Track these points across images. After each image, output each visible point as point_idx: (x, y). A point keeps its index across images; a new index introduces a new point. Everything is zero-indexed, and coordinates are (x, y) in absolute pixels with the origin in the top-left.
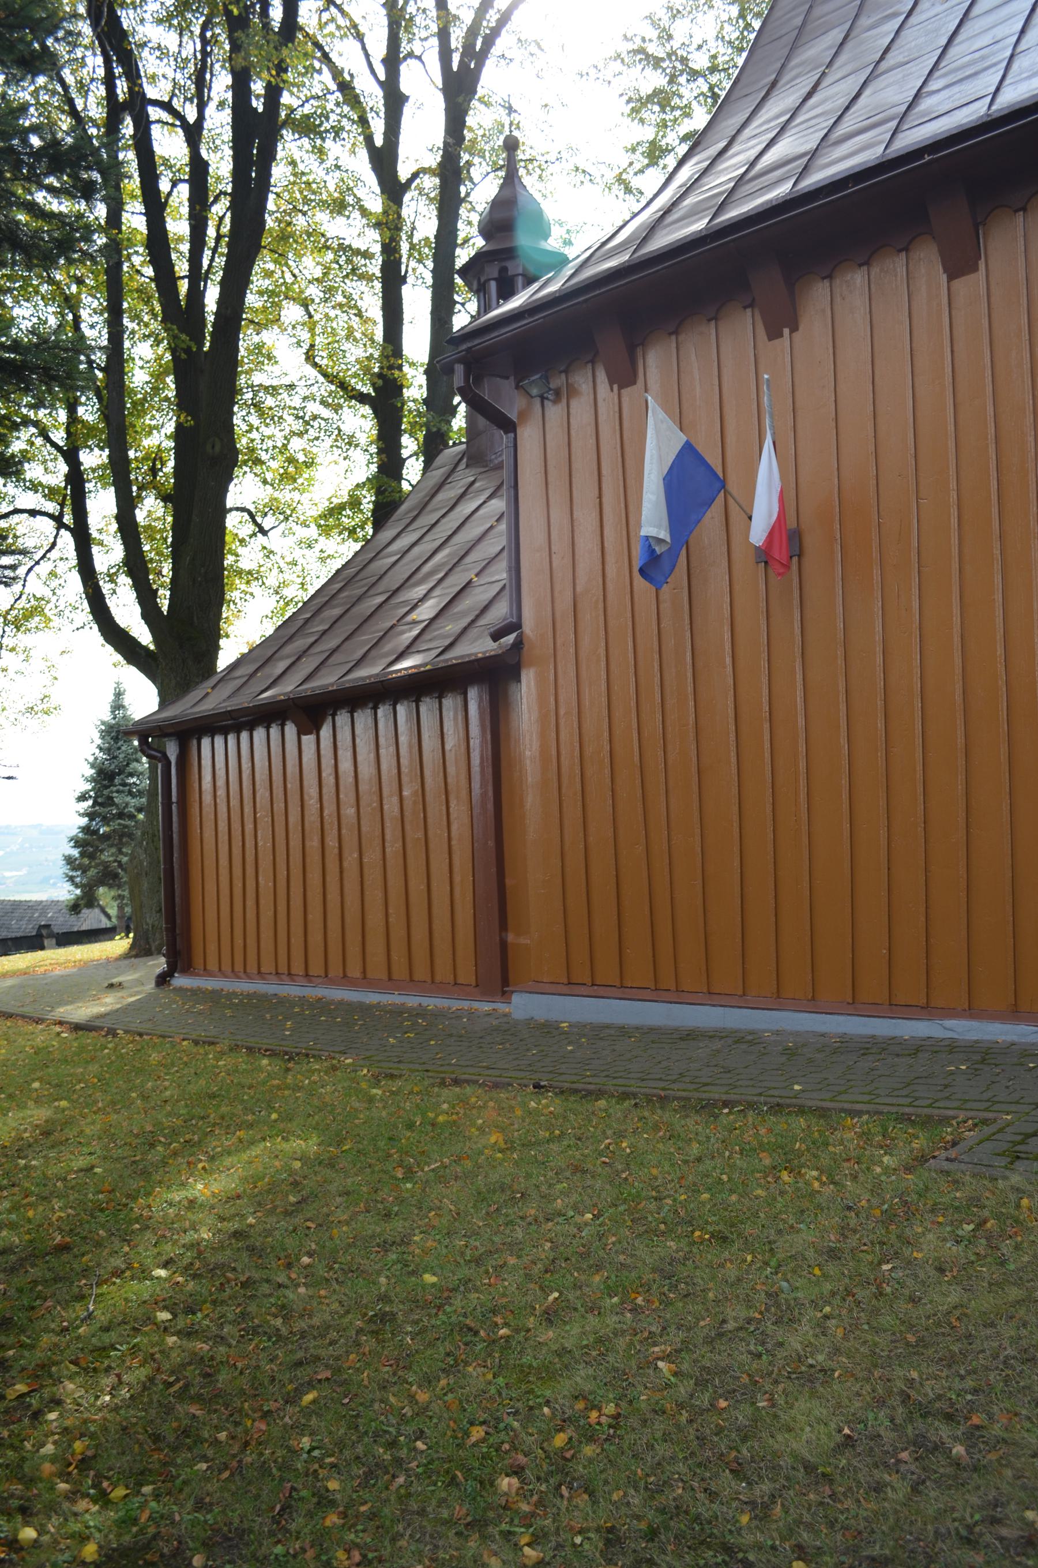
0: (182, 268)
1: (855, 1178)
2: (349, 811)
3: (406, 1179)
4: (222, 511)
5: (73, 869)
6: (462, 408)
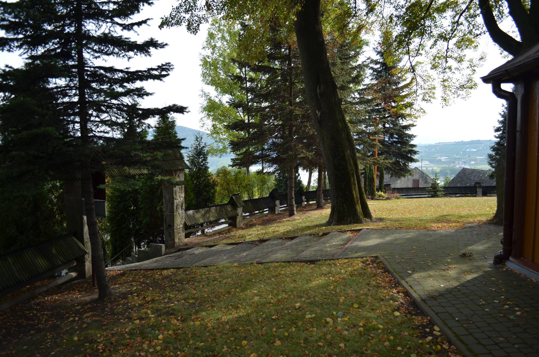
5: (491, 160)
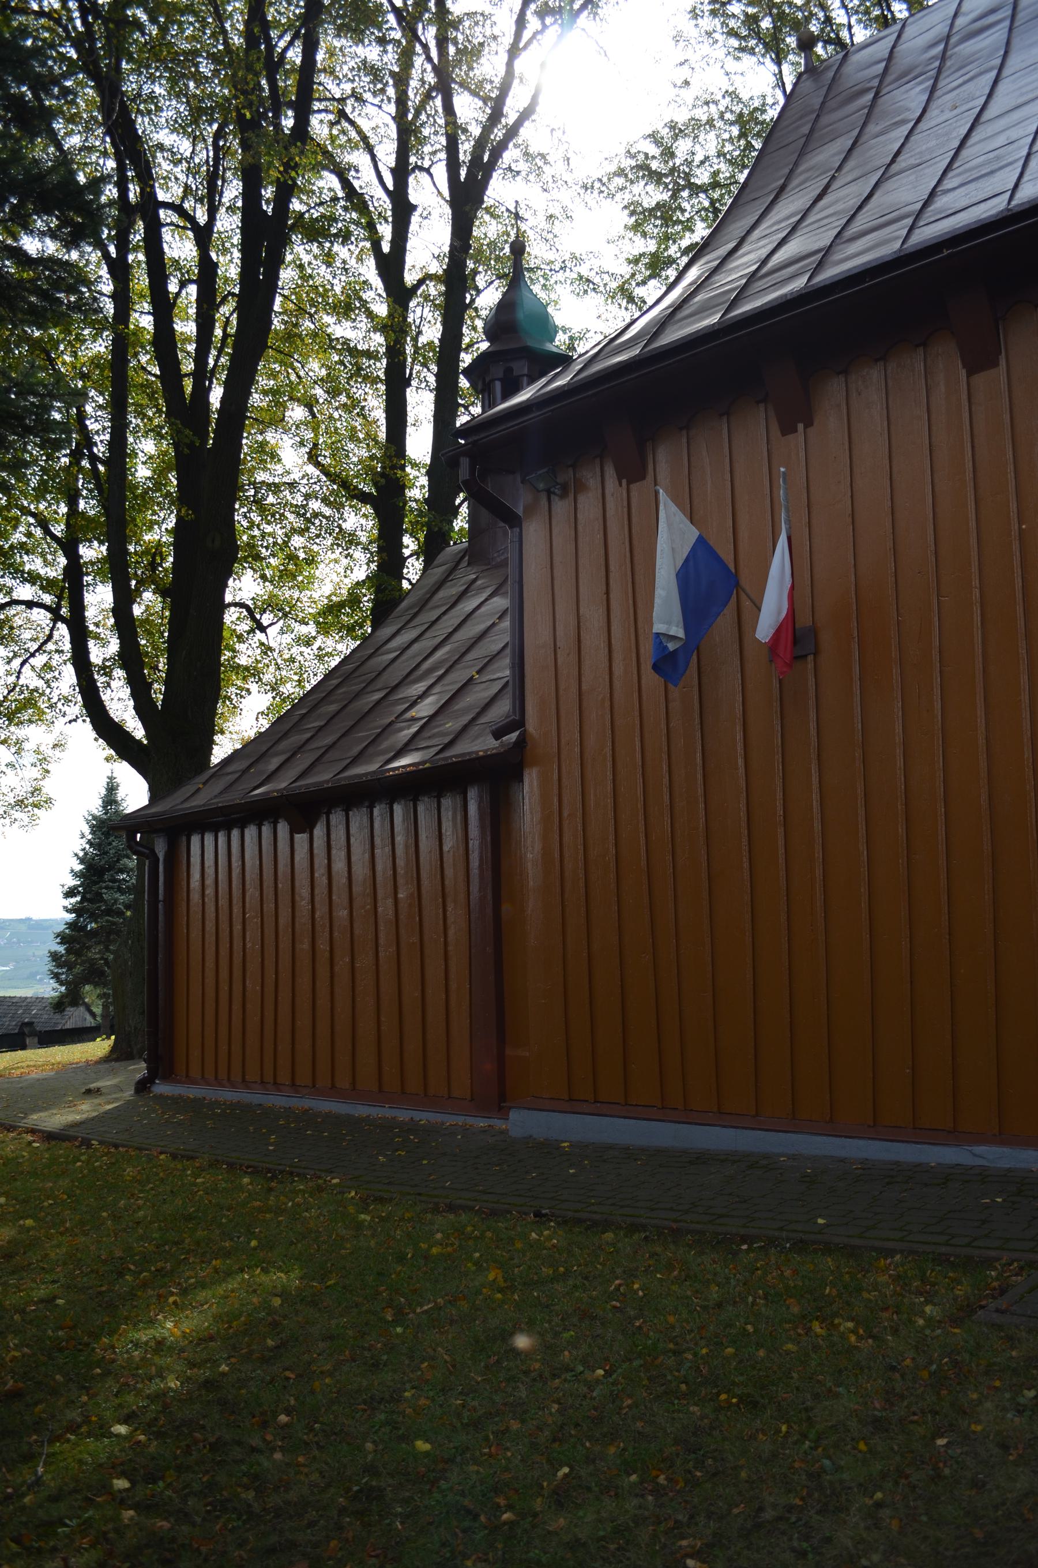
0: (188, 366)
1: (895, 1331)
2: (342, 913)
3: (396, 1322)
4: (222, 607)
5: (58, 966)
6: (464, 510)
